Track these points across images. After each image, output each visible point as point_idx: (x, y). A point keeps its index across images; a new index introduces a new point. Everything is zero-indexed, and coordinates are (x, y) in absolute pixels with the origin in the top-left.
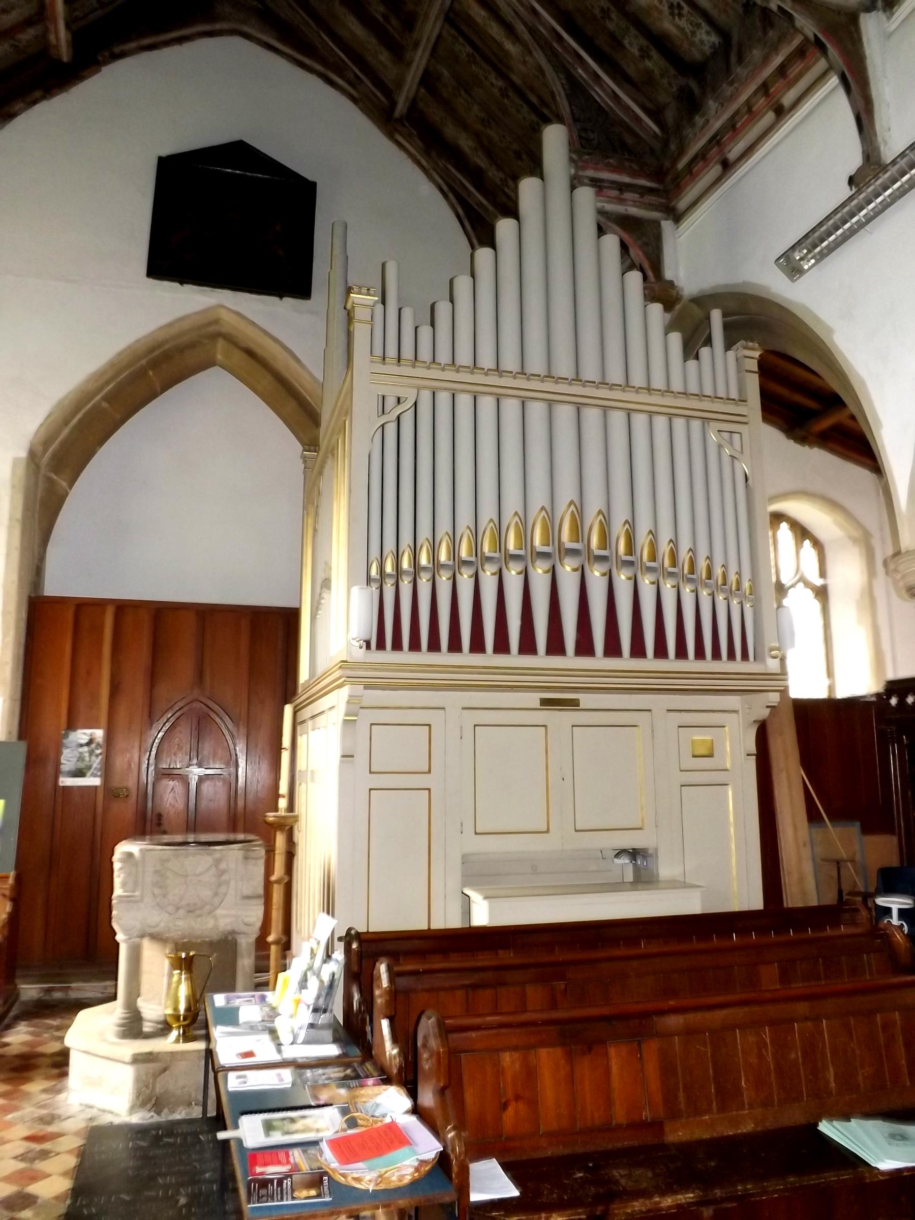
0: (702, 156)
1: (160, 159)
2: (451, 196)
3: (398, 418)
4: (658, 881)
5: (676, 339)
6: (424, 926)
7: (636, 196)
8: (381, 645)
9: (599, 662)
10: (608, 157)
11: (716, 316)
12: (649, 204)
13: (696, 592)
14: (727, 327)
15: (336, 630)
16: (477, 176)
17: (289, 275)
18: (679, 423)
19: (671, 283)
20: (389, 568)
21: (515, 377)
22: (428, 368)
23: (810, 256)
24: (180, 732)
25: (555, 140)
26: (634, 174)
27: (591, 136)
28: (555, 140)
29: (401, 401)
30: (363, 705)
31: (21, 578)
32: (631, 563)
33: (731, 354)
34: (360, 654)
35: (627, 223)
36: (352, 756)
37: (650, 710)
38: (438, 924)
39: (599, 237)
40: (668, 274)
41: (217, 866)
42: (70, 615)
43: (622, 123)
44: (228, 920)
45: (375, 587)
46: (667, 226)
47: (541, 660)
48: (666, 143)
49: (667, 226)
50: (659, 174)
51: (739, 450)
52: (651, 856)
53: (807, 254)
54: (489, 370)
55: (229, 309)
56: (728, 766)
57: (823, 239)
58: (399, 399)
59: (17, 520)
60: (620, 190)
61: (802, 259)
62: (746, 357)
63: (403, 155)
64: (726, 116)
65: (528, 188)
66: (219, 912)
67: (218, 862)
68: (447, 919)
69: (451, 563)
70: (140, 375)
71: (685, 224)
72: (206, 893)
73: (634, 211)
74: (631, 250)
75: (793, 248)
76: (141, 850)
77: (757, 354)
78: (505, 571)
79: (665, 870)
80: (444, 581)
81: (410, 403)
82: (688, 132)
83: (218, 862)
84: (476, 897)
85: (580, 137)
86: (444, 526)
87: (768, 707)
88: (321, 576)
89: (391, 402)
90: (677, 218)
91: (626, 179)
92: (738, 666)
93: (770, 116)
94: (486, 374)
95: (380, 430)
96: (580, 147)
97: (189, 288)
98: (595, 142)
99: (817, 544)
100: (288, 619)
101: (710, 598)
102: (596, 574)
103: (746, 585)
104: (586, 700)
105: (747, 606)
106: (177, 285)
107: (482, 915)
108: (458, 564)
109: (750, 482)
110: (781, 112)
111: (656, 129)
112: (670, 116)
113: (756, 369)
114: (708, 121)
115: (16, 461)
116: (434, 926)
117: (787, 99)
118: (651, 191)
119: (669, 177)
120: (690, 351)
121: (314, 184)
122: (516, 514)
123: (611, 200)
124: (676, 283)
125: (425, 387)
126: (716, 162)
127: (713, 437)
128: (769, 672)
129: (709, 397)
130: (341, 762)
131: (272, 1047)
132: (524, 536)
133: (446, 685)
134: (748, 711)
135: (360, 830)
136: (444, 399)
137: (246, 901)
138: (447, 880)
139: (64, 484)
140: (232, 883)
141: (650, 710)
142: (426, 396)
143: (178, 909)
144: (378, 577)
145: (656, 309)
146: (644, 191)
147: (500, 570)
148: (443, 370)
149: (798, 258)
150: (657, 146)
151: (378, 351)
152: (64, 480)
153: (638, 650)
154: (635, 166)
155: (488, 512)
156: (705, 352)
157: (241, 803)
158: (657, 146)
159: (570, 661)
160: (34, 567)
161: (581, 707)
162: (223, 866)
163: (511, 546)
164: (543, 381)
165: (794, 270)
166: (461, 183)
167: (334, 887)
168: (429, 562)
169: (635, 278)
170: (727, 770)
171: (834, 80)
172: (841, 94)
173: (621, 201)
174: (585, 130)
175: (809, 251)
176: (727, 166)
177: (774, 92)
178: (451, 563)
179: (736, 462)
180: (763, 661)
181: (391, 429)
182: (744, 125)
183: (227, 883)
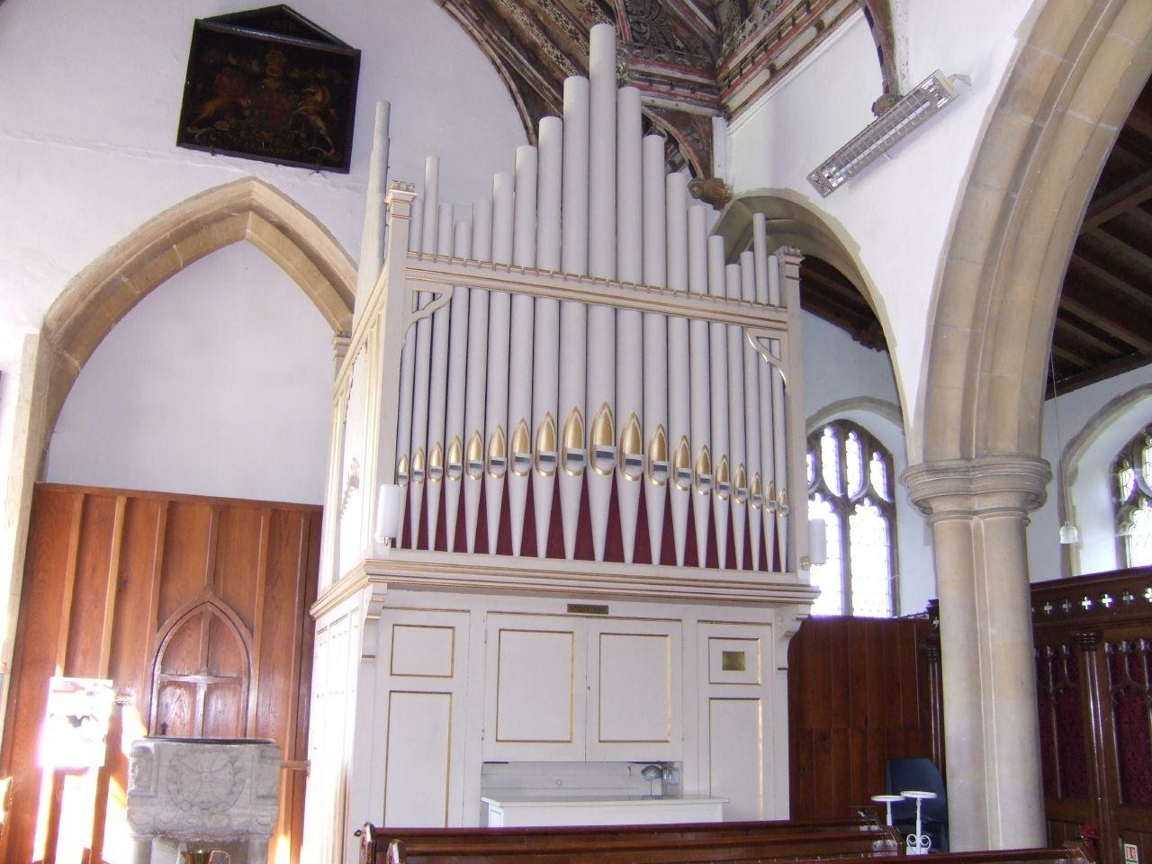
0: (751, 59)
1: (197, 22)
2: (504, 69)
3: (433, 314)
4: (682, 795)
5: (717, 243)
6: (442, 825)
7: (687, 92)
8: (406, 544)
9: (628, 567)
10: (659, 52)
11: (759, 222)
12: (700, 100)
13: (761, 508)
14: (770, 230)
15: (356, 532)
16: (532, 52)
17: (323, 141)
18: (718, 329)
19: (720, 182)
20: (417, 466)
21: (551, 277)
22: (465, 265)
23: (838, 174)
24: (190, 636)
25: (601, 39)
26: (686, 70)
27: (644, 29)
28: (601, 39)
29: (437, 296)
30: (386, 604)
31: (27, 464)
32: (664, 469)
33: (773, 259)
34: (385, 551)
35: (676, 117)
36: (374, 657)
37: (680, 620)
38: (457, 822)
39: (643, 136)
40: (718, 173)
41: (233, 764)
42: (78, 506)
43: (676, 17)
44: (242, 820)
45: (402, 483)
46: (718, 122)
47: (569, 564)
48: (720, 39)
49: (718, 122)
50: (712, 71)
51: (778, 357)
52: (677, 770)
53: (835, 173)
54: (526, 268)
55: (262, 182)
56: (759, 681)
57: (857, 158)
58: (434, 295)
59: (27, 401)
60: (672, 86)
61: (828, 177)
62: (787, 263)
63: (457, 26)
64: (773, 25)
65: (572, 86)
66: (232, 810)
67: (233, 761)
68: (464, 818)
69: (480, 462)
70: (163, 247)
71: (734, 125)
72: (221, 791)
73: (685, 107)
74: (681, 145)
75: (823, 168)
76: (155, 746)
77: (799, 260)
78: (535, 472)
79: (689, 786)
80: (472, 479)
81: (445, 299)
82: (738, 35)
83: (233, 761)
84: (493, 805)
85: (632, 29)
86: (475, 423)
87: (797, 619)
88: (348, 472)
89: (426, 298)
90: (729, 118)
91: (679, 75)
92: (770, 577)
93: (812, 31)
94: (523, 273)
95: (414, 326)
96: (632, 40)
97: (221, 158)
98: (647, 36)
99: (887, 458)
100: (313, 516)
101: (743, 507)
102: (628, 479)
103: (780, 494)
104: (615, 608)
105: (781, 516)
106: (208, 155)
107: (497, 820)
108: (487, 464)
109: (786, 389)
110: (822, 30)
111: (711, 26)
112: (724, 12)
113: (798, 276)
114: (756, 26)
115: (28, 337)
116: (451, 825)
117: (828, 18)
118: (702, 87)
119: (722, 75)
120: (732, 257)
121: (359, 52)
122: (576, 409)
123: (660, 94)
124: (725, 182)
125: (461, 285)
126: (763, 68)
127: (751, 343)
128: (800, 583)
129: (749, 302)
130: (362, 662)
131: (425, 320)
132: (584, 435)
133: (470, 586)
134: (780, 624)
135: (377, 738)
136: (479, 297)
137: (261, 801)
138: (468, 781)
139: (76, 363)
140: (248, 781)
141: (680, 620)
142: (461, 294)
143: (192, 805)
144: (406, 474)
145: (700, 210)
146: (696, 87)
147: (531, 471)
148: (480, 267)
149: (826, 176)
150: (711, 41)
151: (415, 247)
152: (77, 359)
153: (668, 558)
154: (687, 62)
155: (572, 400)
156: (746, 256)
157: (251, 724)
158: (711, 41)
159: (599, 566)
160: (40, 456)
161: (611, 613)
162: (238, 764)
163: (543, 446)
164: (580, 282)
165: (823, 186)
166: (516, 57)
167: (349, 793)
168: (458, 460)
169: (680, 180)
170: (758, 684)
171: (860, 13)
172: (865, 23)
173: (672, 96)
174: (639, 23)
175: (840, 168)
176: (775, 72)
177: (815, 8)
178: (480, 462)
179: (774, 369)
180: (795, 572)
181: (425, 326)
182: (737, 84)
183: (243, 782)
